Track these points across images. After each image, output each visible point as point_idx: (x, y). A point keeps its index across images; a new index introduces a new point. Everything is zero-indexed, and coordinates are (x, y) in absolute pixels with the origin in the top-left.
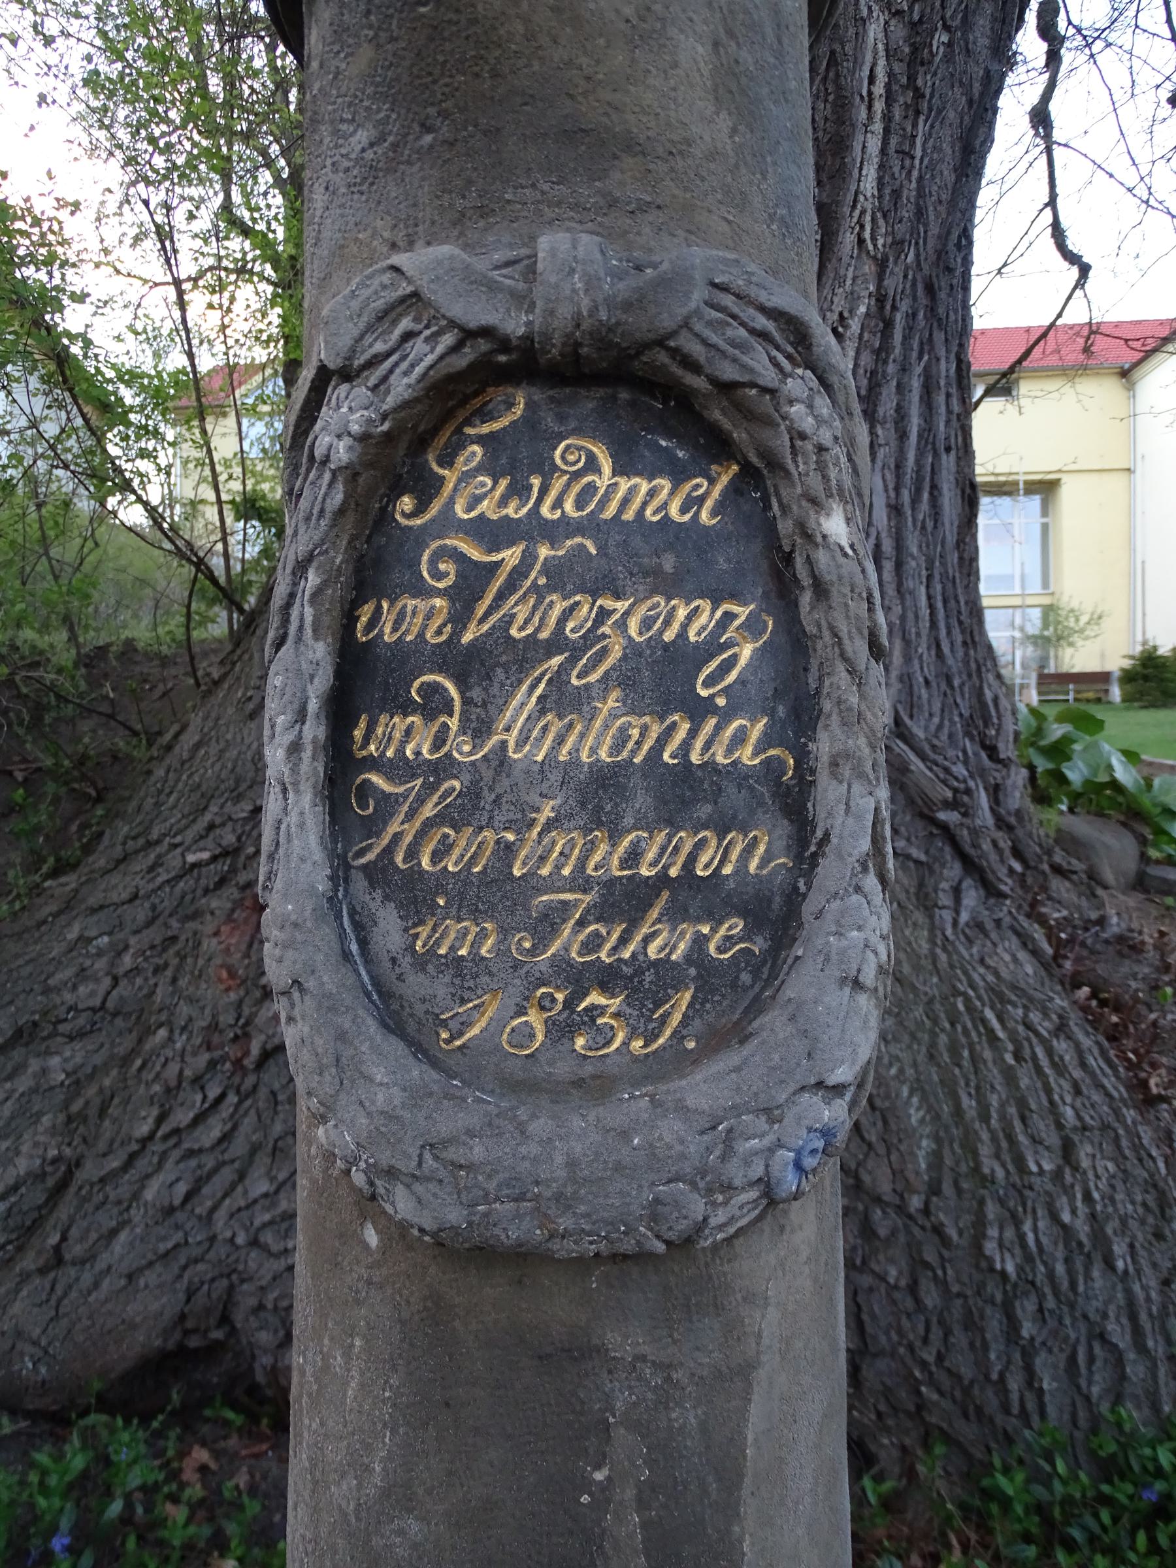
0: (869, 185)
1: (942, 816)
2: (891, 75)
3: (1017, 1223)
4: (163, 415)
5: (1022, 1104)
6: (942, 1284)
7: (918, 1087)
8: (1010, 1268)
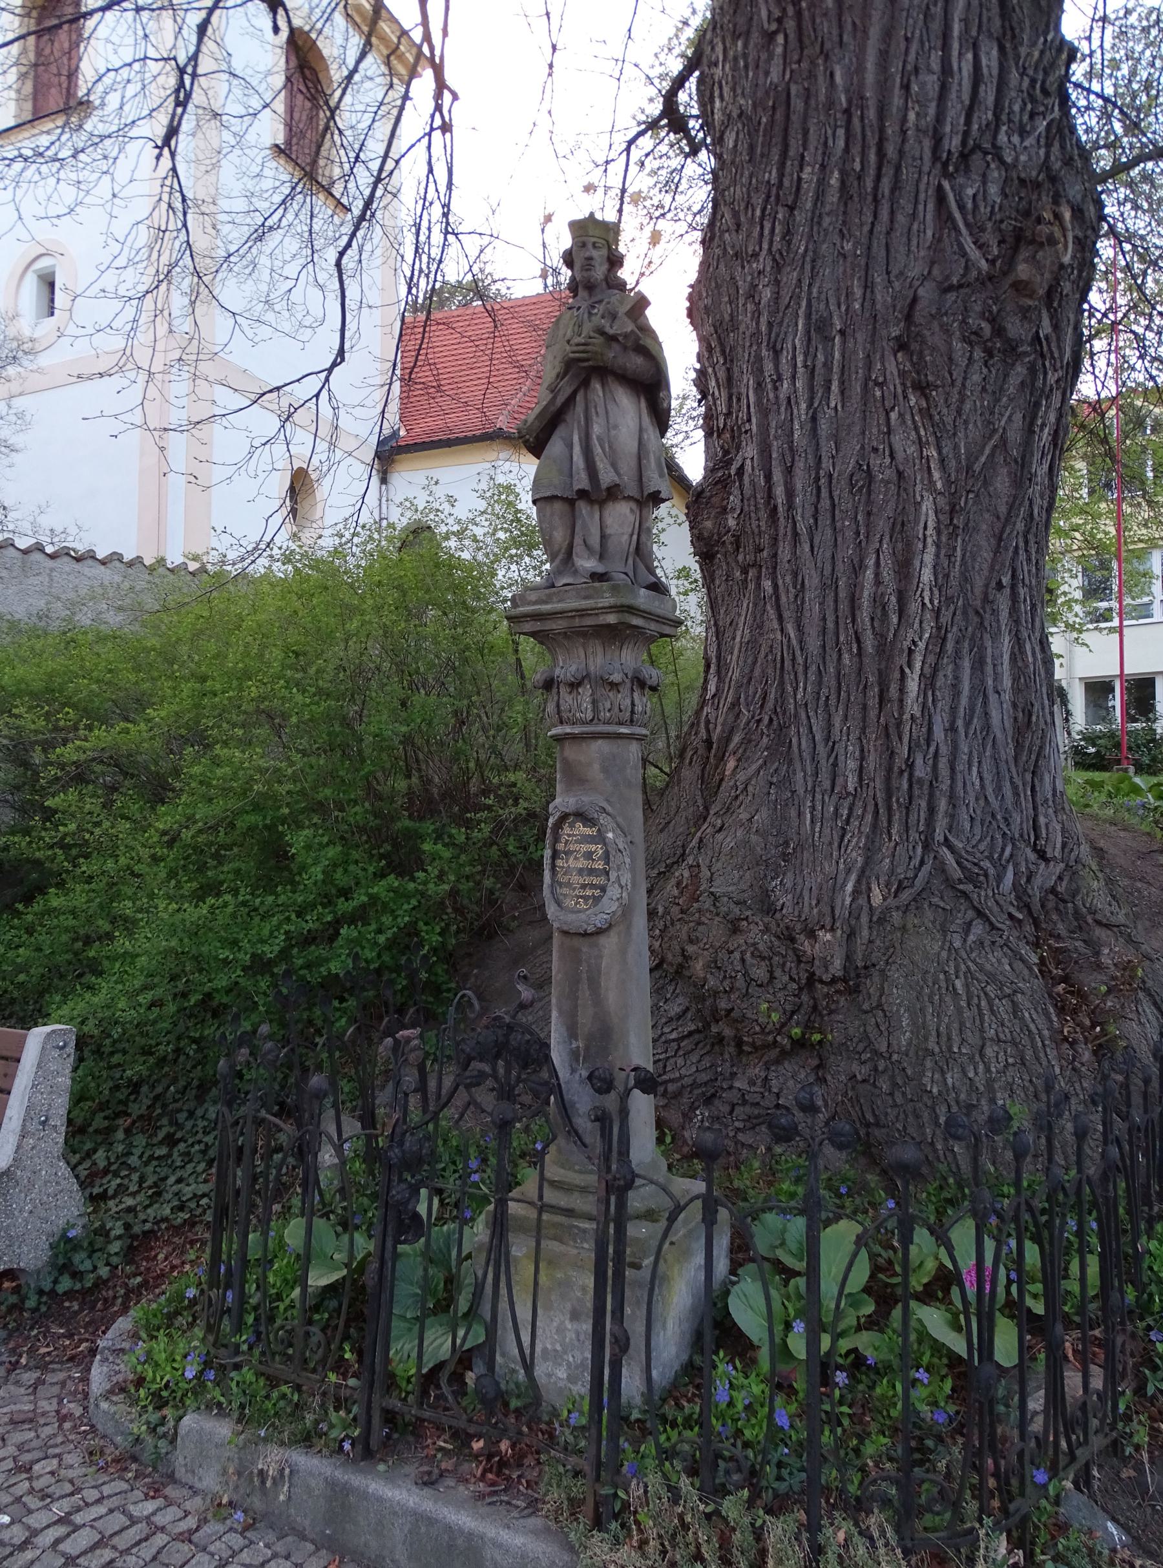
0: (927, 575)
1: (961, 887)
2: (938, 522)
3: (943, 1073)
4: (1126, 199)
5: (962, 1024)
6: (904, 1094)
7: (908, 1010)
8: (935, 1090)
